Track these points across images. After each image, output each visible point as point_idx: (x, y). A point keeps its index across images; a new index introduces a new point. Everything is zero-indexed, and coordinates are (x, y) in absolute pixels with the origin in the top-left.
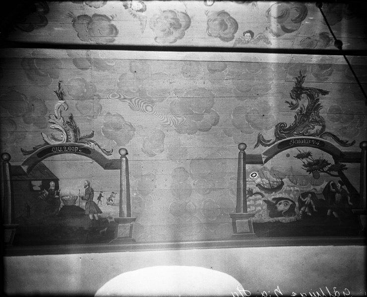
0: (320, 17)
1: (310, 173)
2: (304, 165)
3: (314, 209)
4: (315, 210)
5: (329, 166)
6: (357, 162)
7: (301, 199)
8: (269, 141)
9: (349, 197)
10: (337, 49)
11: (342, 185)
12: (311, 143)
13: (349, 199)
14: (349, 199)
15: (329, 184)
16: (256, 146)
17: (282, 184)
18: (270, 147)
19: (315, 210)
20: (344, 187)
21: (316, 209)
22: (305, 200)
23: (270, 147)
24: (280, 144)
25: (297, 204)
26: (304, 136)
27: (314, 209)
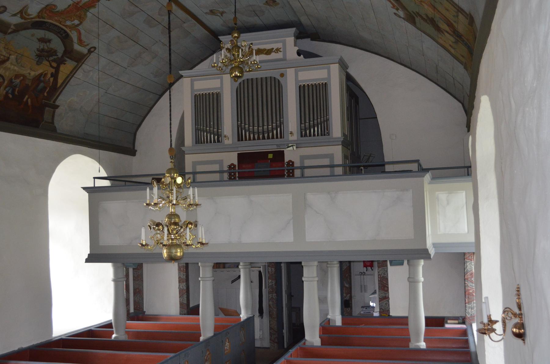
0: (319, 340)
1: (37, 58)
2: (37, 49)
3: (16, 91)
4: (16, 93)
5: (55, 57)
6: (76, 62)
7: (12, 79)
8: (29, 15)
9: (48, 89)
10: (172, 3)
11: (52, 76)
12: (226, 312)
13: (47, 90)
14: (47, 90)
15: (43, 72)
16: (15, 15)
17: (8, 59)
18: (25, 21)
19: (16, 93)
20: (52, 79)
21: (17, 92)
22: (15, 81)
23: (25, 21)
24: (37, 22)
25: (6, 82)
26: (60, 23)
27: (16, 91)
